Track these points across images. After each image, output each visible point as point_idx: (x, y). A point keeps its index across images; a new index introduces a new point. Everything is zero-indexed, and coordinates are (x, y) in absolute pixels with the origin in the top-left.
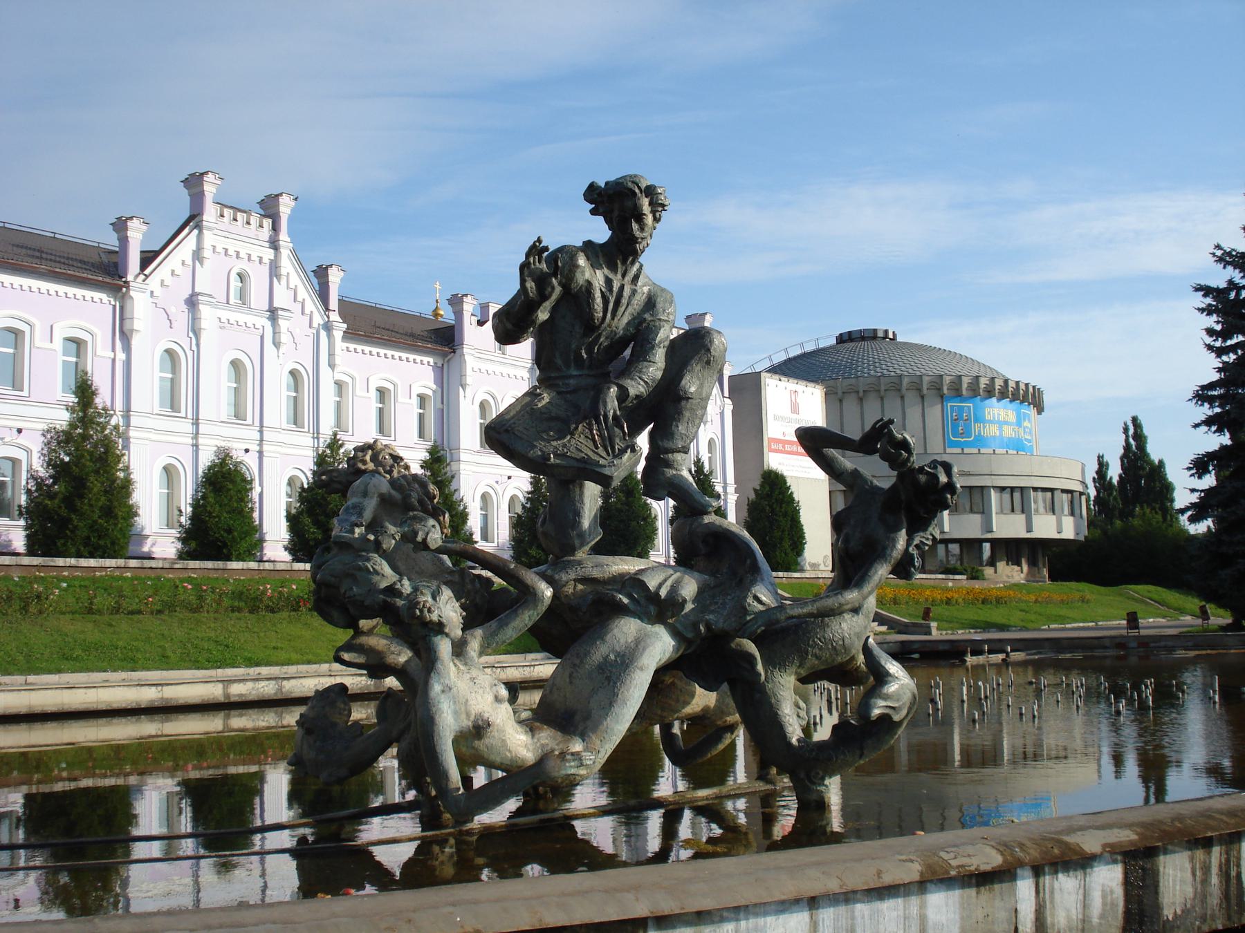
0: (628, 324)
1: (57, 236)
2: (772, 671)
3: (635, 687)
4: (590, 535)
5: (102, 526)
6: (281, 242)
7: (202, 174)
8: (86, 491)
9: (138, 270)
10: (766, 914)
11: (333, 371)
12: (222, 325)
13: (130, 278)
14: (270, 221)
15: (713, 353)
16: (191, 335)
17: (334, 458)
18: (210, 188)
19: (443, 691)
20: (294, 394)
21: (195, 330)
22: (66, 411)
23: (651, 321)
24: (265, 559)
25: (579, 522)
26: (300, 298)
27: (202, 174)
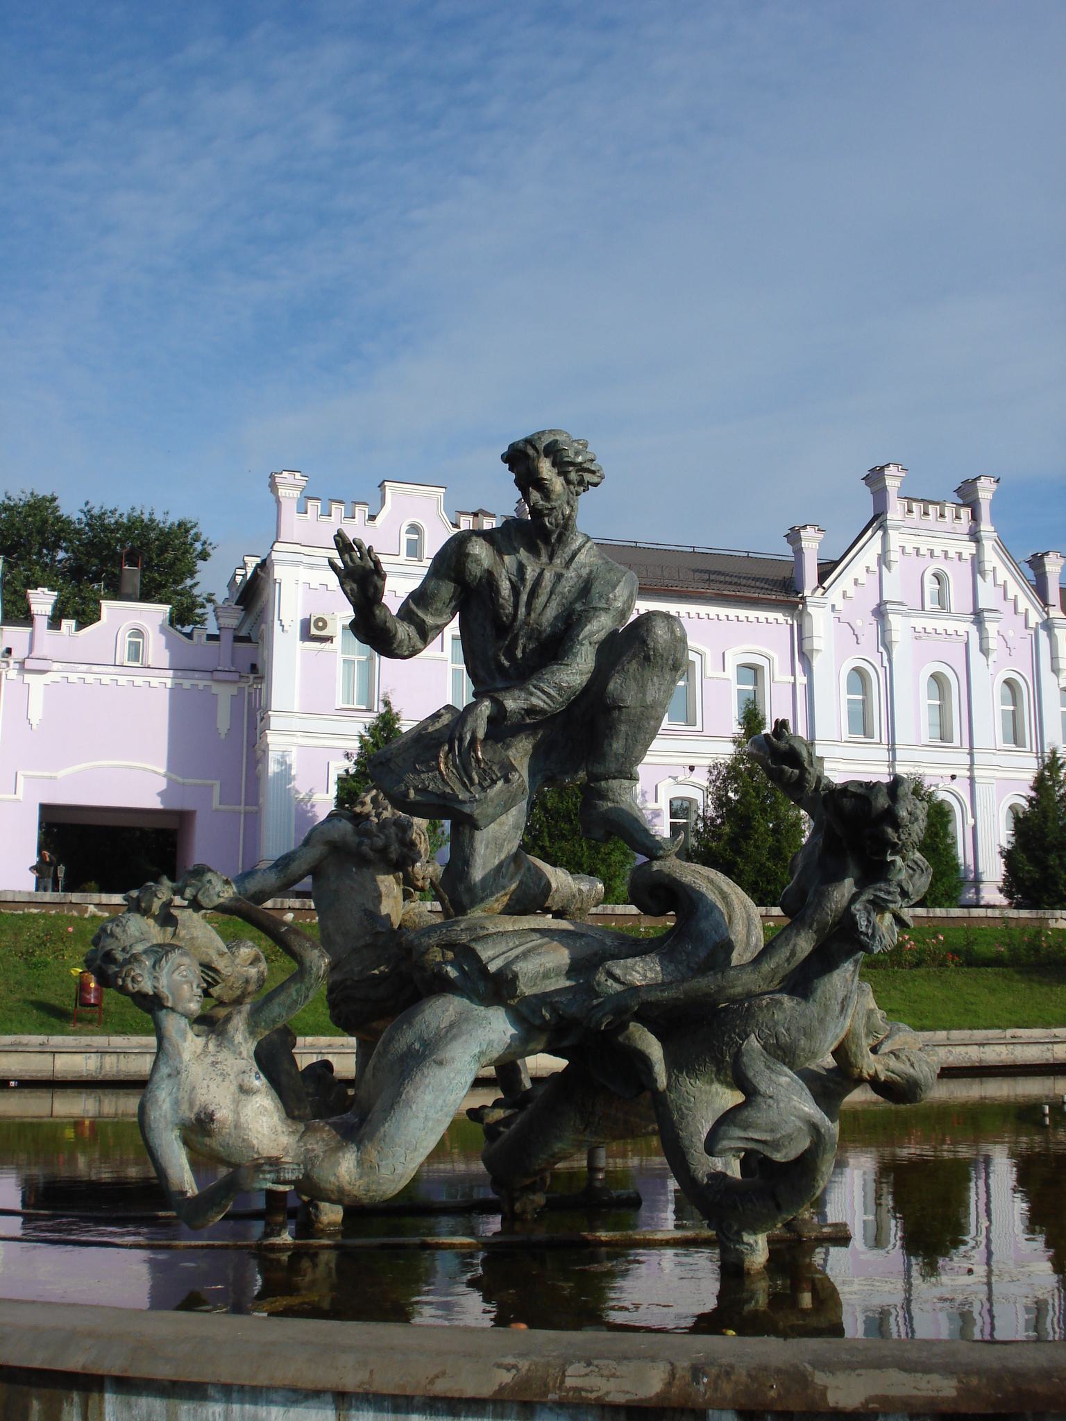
0: (556, 618)
1: (750, 555)
2: (677, 1077)
3: (427, 1086)
4: (484, 889)
5: (769, 869)
6: (982, 533)
7: (883, 468)
8: (751, 831)
9: (816, 583)
10: (270, 1402)
11: (1058, 677)
12: (917, 635)
13: (807, 592)
14: (969, 510)
15: (652, 645)
16: (881, 649)
17: (1054, 781)
18: (892, 483)
19: (169, 1075)
20: (1012, 708)
21: (886, 643)
22: (731, 744)
23: (582, 611)
24: (982, 903)
25: (468, 873)
26: (1010, 596)
27: (883, 468)
